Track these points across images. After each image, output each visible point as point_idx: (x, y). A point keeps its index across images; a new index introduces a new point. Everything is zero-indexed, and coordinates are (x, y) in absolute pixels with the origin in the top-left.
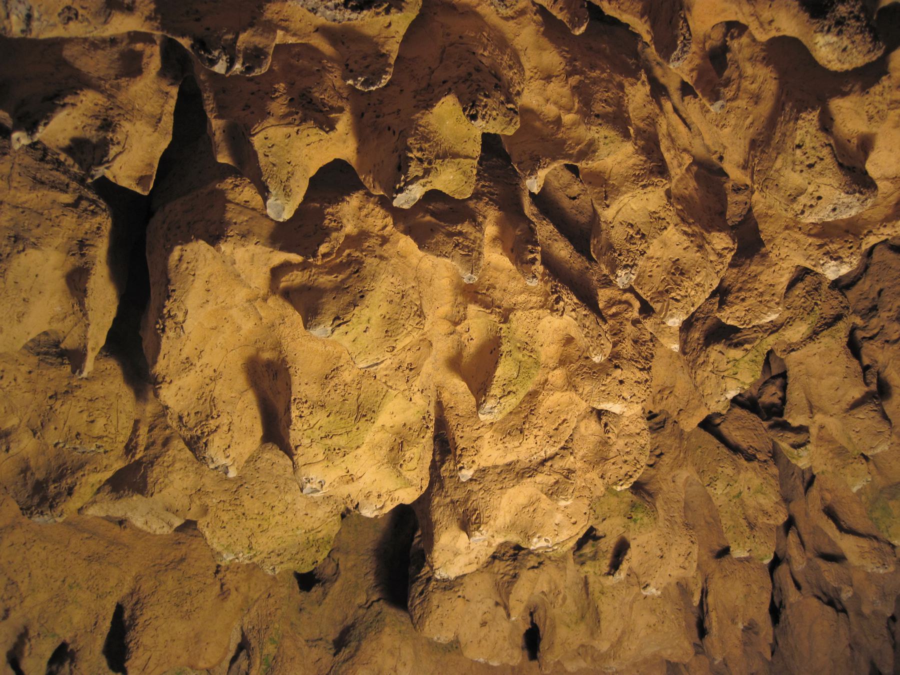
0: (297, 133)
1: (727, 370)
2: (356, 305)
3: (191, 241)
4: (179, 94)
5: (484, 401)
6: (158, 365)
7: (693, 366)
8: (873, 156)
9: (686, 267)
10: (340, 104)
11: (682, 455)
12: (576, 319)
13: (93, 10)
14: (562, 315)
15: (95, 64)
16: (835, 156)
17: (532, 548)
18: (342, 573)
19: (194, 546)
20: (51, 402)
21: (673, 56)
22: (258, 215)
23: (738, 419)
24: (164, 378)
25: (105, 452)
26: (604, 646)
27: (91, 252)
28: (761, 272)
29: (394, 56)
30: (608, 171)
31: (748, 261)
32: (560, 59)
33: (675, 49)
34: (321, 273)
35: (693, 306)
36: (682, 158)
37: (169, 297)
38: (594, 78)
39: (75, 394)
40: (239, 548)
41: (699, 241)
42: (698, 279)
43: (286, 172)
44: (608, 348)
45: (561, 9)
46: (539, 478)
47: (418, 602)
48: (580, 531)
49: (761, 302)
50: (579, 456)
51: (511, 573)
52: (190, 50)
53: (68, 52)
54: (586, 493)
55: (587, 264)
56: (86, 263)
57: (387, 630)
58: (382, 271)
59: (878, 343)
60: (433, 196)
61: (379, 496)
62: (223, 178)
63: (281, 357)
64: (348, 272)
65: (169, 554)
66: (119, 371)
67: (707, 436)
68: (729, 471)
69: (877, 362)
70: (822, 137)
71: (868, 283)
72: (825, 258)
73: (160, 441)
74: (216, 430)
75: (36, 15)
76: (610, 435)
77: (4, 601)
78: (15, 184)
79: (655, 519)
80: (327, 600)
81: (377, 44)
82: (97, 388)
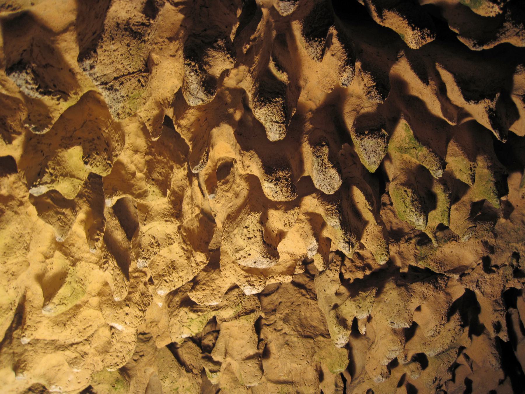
1: (186, 322)
7: (171, 314)
8: (284, 241)
9: (177, 266)
11: (153, 359)
12: (112, 275)
14: (105, 271)
16: (263, 237)
21: (195, 168)
23: (190, 348)
28: (217, 279)
29: (56, 120)
31: (213, 271)
32: (146, 145)
33: (197, 165)
35: (174, 287)
36: (195, 210)
38: (159, 160)
41: (188, 254)
42: (181, 274)
44: (125, 294)
45: (150, 125)
49: (212, 294)
50: (93, 346)
54: (92, 367)
59: (271, 329)
67: (169, 353)
68: (175, 375)
69: (267, 338)
70: (259, 226)
71: (276, 296)
72: (246, 283)
76: (113, 340)
79: (127, 390)
81: (49, 111)
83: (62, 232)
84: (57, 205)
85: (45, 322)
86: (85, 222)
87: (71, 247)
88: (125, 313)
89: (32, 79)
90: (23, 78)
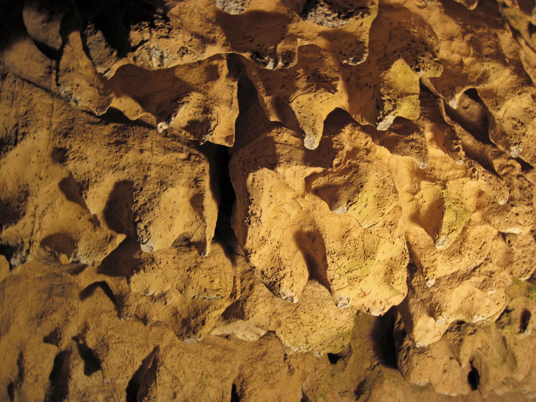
0: (315, 96)
2: (359, 192)
3: (259, 169)
4: (238, 85)
5: (438, 238)
6: (247, 243)
10: (336, 75)
12: (485, 180)
13: (195, 46)
14: (478, 179)
15: (193, 77)
17: (474, 322)
18: (354, 351)
19: (269, 346)
20: (188, 273)
22: (294, 148)
24: (251, 251)
25: (222, 298)
26: (520, 377)
27: (202, 184)
29: (367, 42)
30: (495, 88)
32: (458, 26)
34: (335, 176)
37: (250, 203)
38: (480, 34)
39: (200, 267)
40: (300, 344)
43: (311, 120)
46: (473, 279)
47: (404, 363)
48: (501, 308)
50: (495, 262)
51: (458, 338)
52: (250, 59)
53: (178, 73)
55: (483, 146)
56: (200, 191)
57: (386, 381)
58: (370, 170)
60: (398, 120)
61: (381, 303)
62: (270, 130)
63: (316, 228)
64: (351, 173)
65: (256, 352)
66: (222, 250)
73: (248, 287)
74: (284, 277)
75: (165, 55)
76: (513, 247)
77: (172, 388)
78: (155, 153)
80: (347, 368)
81: (356, 36)
82: (212, 262)
83: (422, 157)
84: (402, 135)
85: (439, 257)
86: (434, 140)
87: (433, 171)
88: (515, 215)
89: (329, 9)
90: (321, 12)
